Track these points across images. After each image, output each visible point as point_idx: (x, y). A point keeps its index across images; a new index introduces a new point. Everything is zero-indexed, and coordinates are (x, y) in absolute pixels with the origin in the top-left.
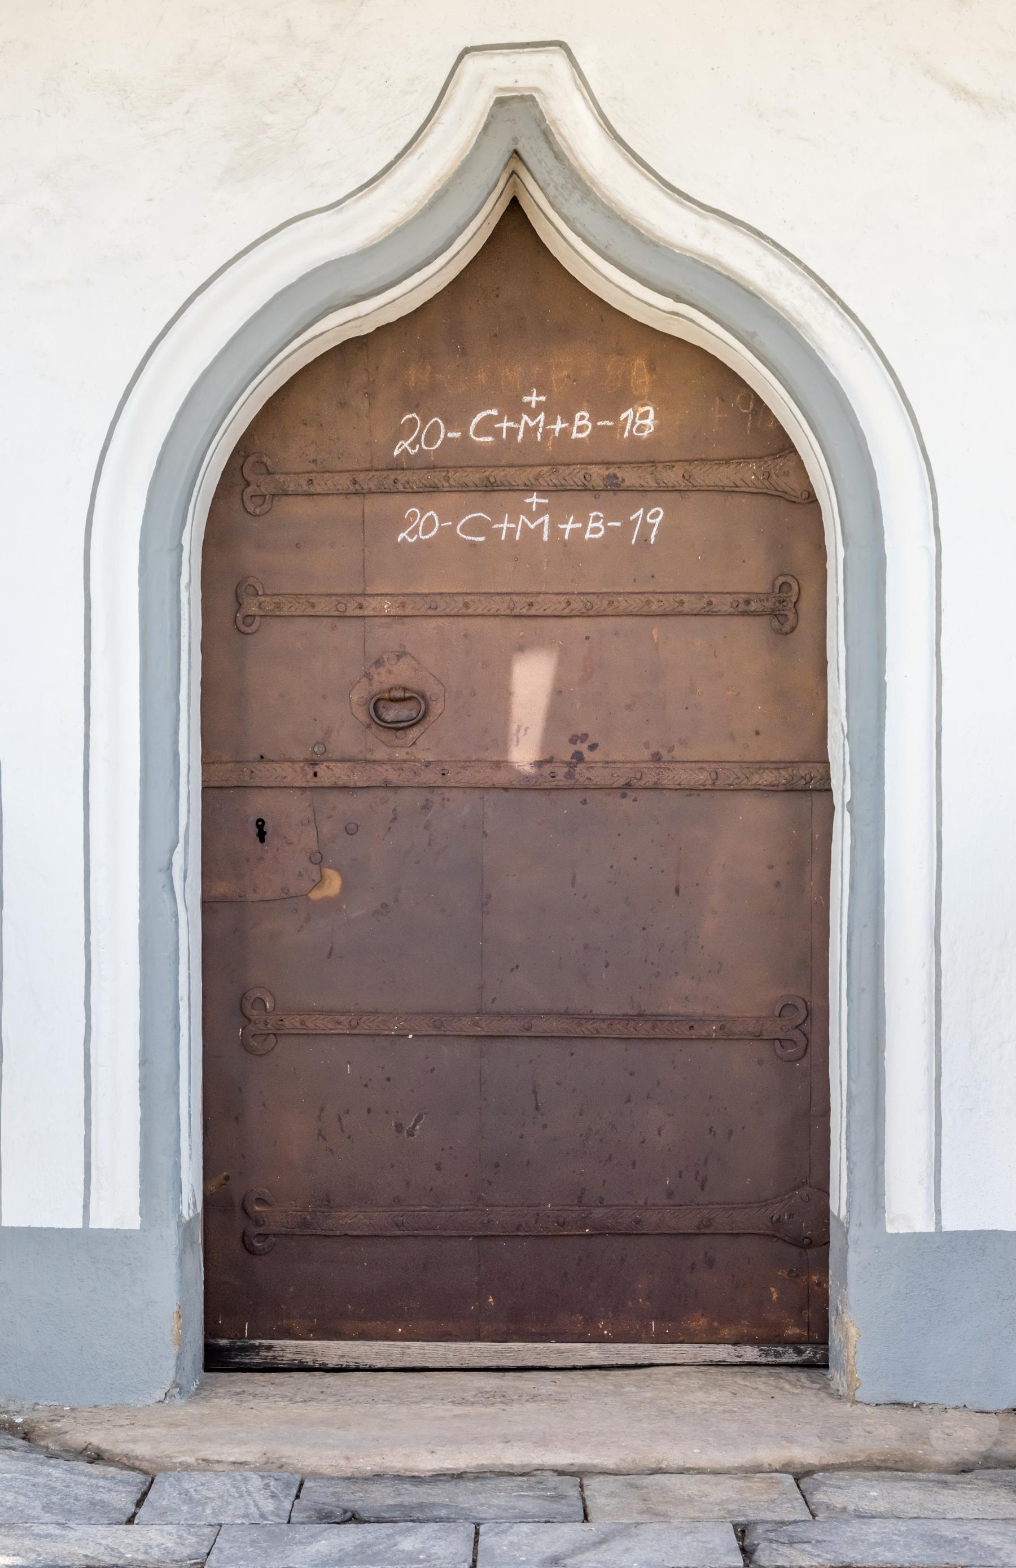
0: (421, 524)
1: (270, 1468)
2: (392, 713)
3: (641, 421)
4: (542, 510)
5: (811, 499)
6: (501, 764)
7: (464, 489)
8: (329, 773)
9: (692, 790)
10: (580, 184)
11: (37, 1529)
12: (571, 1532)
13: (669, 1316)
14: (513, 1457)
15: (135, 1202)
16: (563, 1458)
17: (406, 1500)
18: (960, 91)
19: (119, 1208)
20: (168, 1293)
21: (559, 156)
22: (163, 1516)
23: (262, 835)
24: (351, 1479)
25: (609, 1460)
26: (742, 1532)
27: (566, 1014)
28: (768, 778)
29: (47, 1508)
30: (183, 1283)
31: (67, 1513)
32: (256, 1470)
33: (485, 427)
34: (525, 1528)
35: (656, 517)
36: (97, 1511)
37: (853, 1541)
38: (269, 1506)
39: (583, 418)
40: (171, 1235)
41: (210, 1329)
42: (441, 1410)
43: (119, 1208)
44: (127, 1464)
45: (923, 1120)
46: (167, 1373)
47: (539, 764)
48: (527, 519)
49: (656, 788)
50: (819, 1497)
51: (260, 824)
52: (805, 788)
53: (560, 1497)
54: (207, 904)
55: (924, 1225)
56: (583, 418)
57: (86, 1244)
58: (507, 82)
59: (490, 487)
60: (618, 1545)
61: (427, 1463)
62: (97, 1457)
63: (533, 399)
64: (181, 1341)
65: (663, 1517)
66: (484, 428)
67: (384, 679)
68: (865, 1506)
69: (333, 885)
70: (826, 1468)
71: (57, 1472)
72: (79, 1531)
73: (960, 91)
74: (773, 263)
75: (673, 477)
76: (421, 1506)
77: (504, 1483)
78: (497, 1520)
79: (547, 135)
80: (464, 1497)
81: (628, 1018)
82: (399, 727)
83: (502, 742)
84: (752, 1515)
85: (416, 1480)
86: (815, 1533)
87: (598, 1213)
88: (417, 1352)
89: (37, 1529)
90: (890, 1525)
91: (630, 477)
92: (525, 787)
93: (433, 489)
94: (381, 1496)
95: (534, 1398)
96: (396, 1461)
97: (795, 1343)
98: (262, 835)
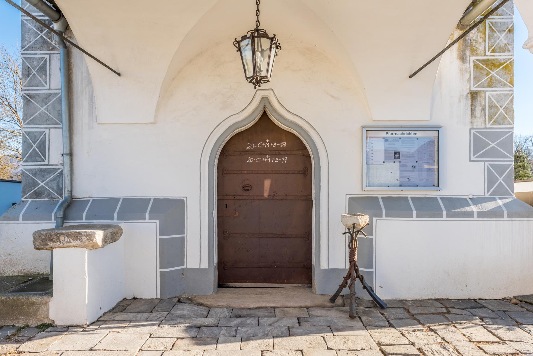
0: (250, 160)
1: (228, 307)
2: (246, 188)
3: (284, 144)
4: (269, 158)
5: (309, 156)
6: (263, 196)
7: (257, 154)
8: (237, 197)
9: (291, 200)
10: (275, 110)
11: (193, 319)
12: (273, 319)
13: (287, 279)
14: (264, 305)
15: (207, 264)
16: (272, 305)
17: (248, 313)
18: (332, 96)
19: (205, 265)
20: (212, 277)
21: (271, 106)
22: (212, 316)
23: (226, 207)
24: (240, 309)
25: (278, 305)
26: (299, 319)
27: (272, 234)
28: (303, 198)
29: (194, 315)
30: (215, 276)
31: (198, 315)
32: (226, 307)
33: (260, 145)
34: (266, 318)
35: (286, 159)
36: (202, 315)
37: (315, 321)
38: (227, 314)
39: (275, 144)
40: (213, 269)
41: (219, 281)
42: (254, 296)
43: (205, 265)
44: (207, 306)
45: (326, 252)
46: (212, 290)
47: (268, 196)
48: (267, 159)
49: (286, 200)
50: (310, 313)
51: (226, 205)
52: (309, 199)
53: (271, 312)
54: (218, 200)
55: (326, 268)
56: (275, 144)
57: (200, 270)
58: (263, 95)
59: (261, 154)
60: (280, 322)
61: (252, 306)
62: (201, 305)
63: (268, 141)
64: (214, 285)
65: (286, 316)
66: (260, 145)
67: (245, 183)
68: (317, 314)
69: (237, 214)
70: (312, 307)
71: (195, 308)
72: (199, 319)
73: (332, 96)
74: (304, 122)
75: (288, 153)
76: (250, 314)
77: (263, 310)
78: (262, 317)
79: (270, 103)
80: (257, 312)
81: (282, 234)
82: (247, 190)
83: (263, 193)
84: (300, 316)
85: (249, 309)
86: (309, 320)
87: (277, 264)
88: (250, 285)
89: (193, 319)
90: (321, 318)
91: (282, 153)
92: (266, 199)
93: (252, 154)
94: (245, 312)
95: (268, 293)
96: (246, 306)
97: (307, 284)
98: (226, 207)
